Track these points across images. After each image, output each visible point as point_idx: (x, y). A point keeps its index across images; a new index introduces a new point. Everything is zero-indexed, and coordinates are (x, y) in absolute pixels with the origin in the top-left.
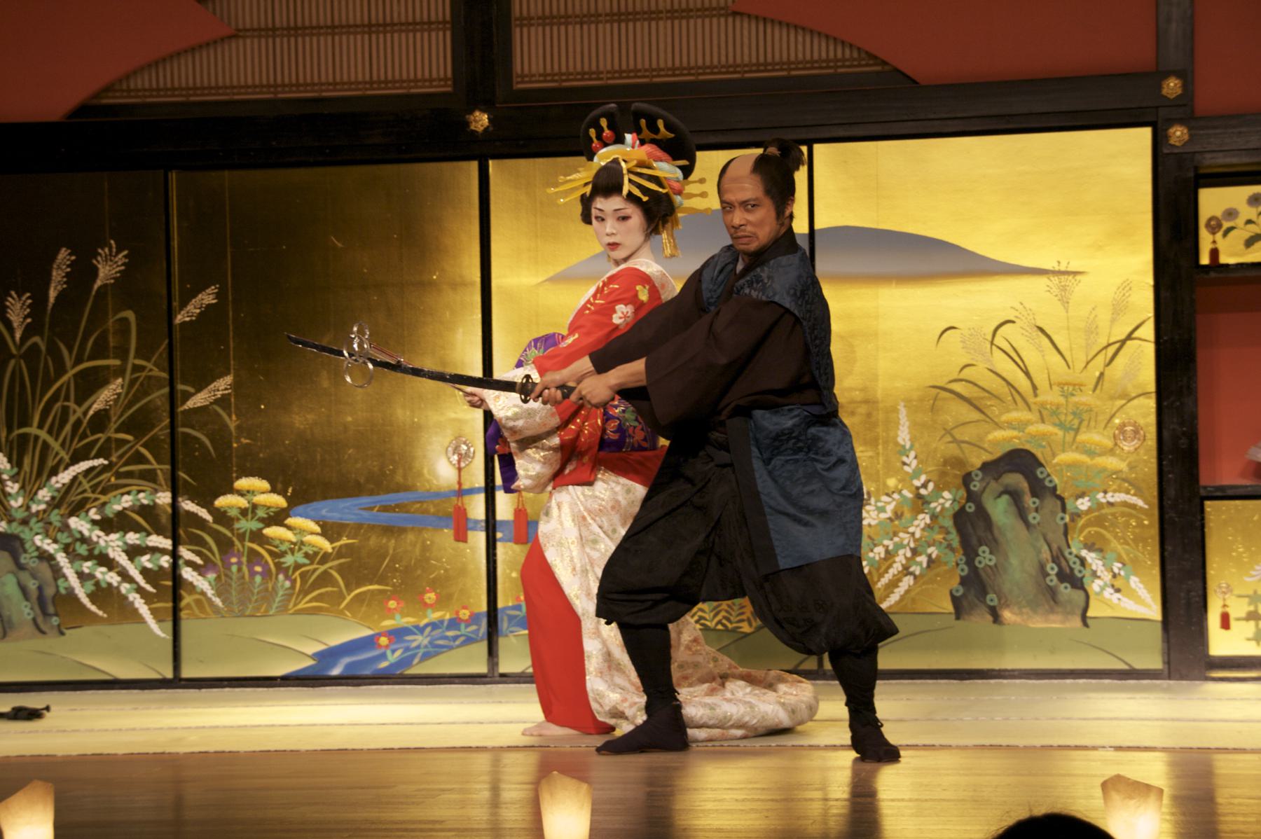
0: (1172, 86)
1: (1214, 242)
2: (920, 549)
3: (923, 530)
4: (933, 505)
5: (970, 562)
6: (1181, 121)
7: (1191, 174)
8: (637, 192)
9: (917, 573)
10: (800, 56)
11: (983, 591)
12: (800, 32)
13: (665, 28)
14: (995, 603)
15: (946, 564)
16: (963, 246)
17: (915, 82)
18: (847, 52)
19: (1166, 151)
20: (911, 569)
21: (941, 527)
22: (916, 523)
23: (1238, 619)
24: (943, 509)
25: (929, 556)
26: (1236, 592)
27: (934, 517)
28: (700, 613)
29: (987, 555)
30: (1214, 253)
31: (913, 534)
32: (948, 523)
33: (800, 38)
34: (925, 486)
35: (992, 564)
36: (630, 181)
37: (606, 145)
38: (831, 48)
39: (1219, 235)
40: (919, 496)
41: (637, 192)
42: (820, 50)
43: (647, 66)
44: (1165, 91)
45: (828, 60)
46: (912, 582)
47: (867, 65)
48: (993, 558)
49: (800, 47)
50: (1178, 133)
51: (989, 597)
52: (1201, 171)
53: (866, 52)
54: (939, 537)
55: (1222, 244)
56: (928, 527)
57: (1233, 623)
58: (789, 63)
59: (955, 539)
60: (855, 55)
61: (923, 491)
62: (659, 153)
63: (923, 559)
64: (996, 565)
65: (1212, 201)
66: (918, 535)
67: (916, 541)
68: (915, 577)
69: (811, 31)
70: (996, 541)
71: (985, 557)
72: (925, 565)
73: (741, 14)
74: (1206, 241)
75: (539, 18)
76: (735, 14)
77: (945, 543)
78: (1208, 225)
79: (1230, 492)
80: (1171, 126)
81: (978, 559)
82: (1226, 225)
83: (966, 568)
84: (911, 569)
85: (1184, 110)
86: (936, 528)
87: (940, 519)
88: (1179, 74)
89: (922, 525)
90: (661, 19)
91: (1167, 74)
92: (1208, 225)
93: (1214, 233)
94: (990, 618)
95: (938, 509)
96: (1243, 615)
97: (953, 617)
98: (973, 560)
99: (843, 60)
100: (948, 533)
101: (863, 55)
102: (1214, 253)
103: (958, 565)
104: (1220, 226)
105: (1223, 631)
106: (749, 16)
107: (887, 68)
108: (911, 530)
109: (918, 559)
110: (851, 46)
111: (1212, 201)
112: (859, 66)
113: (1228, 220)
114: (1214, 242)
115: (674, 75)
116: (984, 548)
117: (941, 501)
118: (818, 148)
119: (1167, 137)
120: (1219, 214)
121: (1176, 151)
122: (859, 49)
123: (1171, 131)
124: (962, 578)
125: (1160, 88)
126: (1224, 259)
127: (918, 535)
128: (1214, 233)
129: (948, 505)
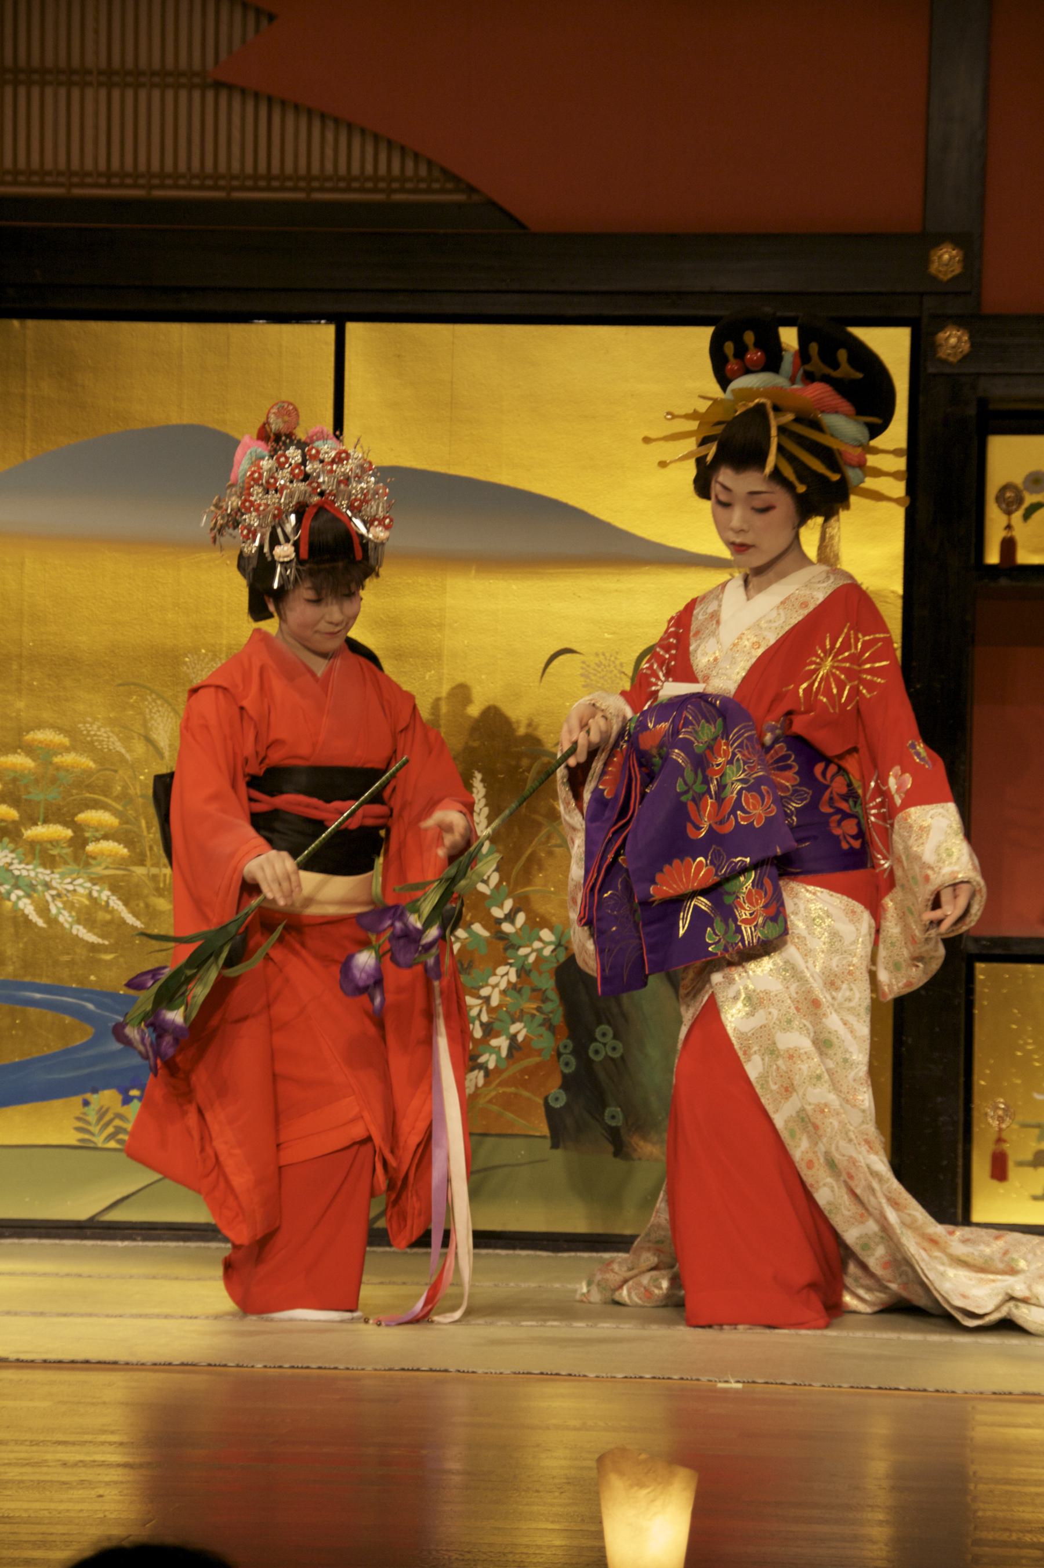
0: (946, 259)
1: (1009, 527)
2: (497, 1026)
3: (503, 993)
4: (523, 951)
5: (580, 1052)
6: (960, 321)
7: (972, 411)
8: (788, 472)
9: (491, 1065)
10: (236, 166)
11: (599, 1102)
12: (330, 125)
13: (96, 101)
14: (618, 1122)
15: (539, 1052)
16: (592, 511)
17: (521, 225)
18: (410, 165)
19: (931, 370)
20: (482, 1060)
21: (534, 990)
22: (493, 980)
23: (1020, 1164)
24: (540, 959)
25: (513, 1038)
26: (1020, 1118)
27: (523, 972)
28: (117, 1122)
29: (609, 1039)
30: (1009, 546)
31: (487, 999)
32: (547, 983)
33: (330, 136)
34: (510, 917)
35: (616, 1055)
36: (780, 448)
37: (747, 371)
38: (383, 157)
39: (1017, 516)
40: (502, 936)
41: (788, 472)
42: (361, 159)
43: (62, 165)
44: (934, 268)
45: (376, 178)
46: (481, 1082)
47: (442, 191)
48: (620, 1045)
49: (329, 152)
50: (953, 341)
51: (608, 1112)
52: (991, 407)
53: (444, 171)
54: (531, 1006)
55: (1022, 532)
56: (513, 988)
57: (1012, 1171)
58: (309, 178)
59: (554, 1006)
60: (423, 172)
61: (507, 927)
62: (838, 401)
63: (501, 1043)
64: (622, 1058)
65: (1010, 458)
66: (495, 1002)
67: (491, 1010)
68: (488, 1073)
69: (350, 126)
70: (625, 1016)
71: (604, 1046)
72: (504, 1053)
73: (230, 87)
74: (996, 524)
75: (100, 73)
76: (218, 85)
77: (540, 1017)
78: (1000, 498)
79: (1016, 950)
80: (942, 328)
81: (593, 1046)
82: (1030, 499)
83: (573, 1061)
84: (482, 1060)
85: (961, 302)
86: (527, 991)
87: (534, 975)
88: (958, 240)
89: (503, 985)
90: (90, 84)
91: (939, 239)
92: (1000, 498)
93: (1009, 513)
94: (611, 1148)
95: (532, 958)
96: (1029, 1156)
97: (548, 1143)
98: (586, 1049)
99: (403, 179)
100: (545, 1000)
101: (436, 173)
102: (1009, 546)
103: (559, 1055)
104: (1020, 501)
105: (995, 1183)
106: (243, 92)
107: (475, 198)
108: (484, 992)
109: (494, 1042)
110: (416, 156)
111: (1010, 458)
112: (429, 191)
113: (1032, 492)
114: (1009, 527)
115: (109, 185)
116: (604, 1027)
117: (537, 945)
118: (354, 330)
119: (934, 347)
120: (1018, 480)
121: (947, 370)
122: (430, 163)
123: (942, 336)
124: (564, 1076)
125: (926, 261)
126: (1025, 557)
127: (495, 1002)
128: (1009, 513)
129: (547, 952)
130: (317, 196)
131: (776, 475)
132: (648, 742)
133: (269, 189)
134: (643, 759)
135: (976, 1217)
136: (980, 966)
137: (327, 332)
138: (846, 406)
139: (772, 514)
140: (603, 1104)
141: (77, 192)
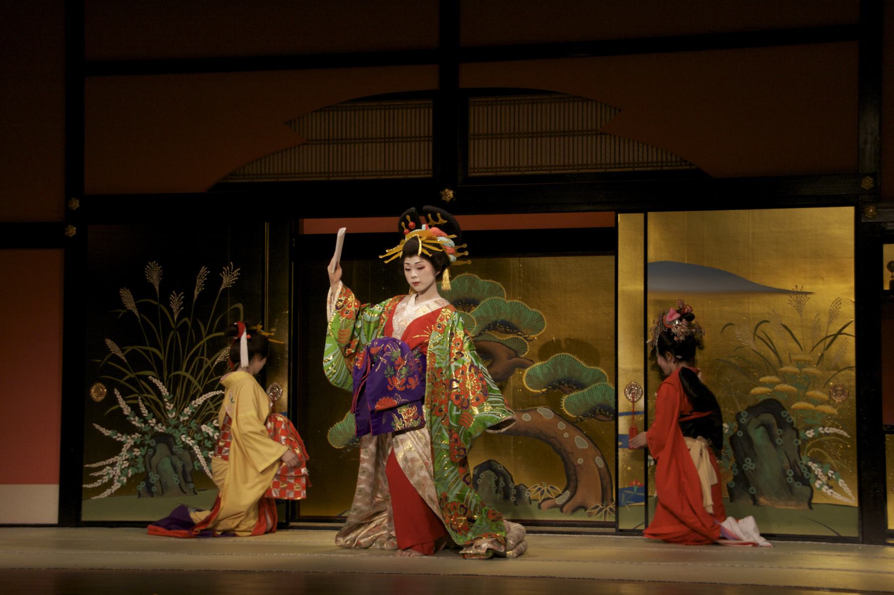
11: (747, 485)
14: (755, 492)
19: (863, 221)
29: (750, 463)
35: (753, 468)
51: (751, 489)
70: (755, 454)
76: (601, 134)
118: (649, 213)
130: (636, 169)
131: (423, 256)
132: (373, 351)
133: (620, 168)
134: (371, 356)
135: (85, 518)
136: (887, 435)
137: (642, 216)
138: (444, 233)
139: (423, 271)
140: (749, 486)
141: (553, 172)
